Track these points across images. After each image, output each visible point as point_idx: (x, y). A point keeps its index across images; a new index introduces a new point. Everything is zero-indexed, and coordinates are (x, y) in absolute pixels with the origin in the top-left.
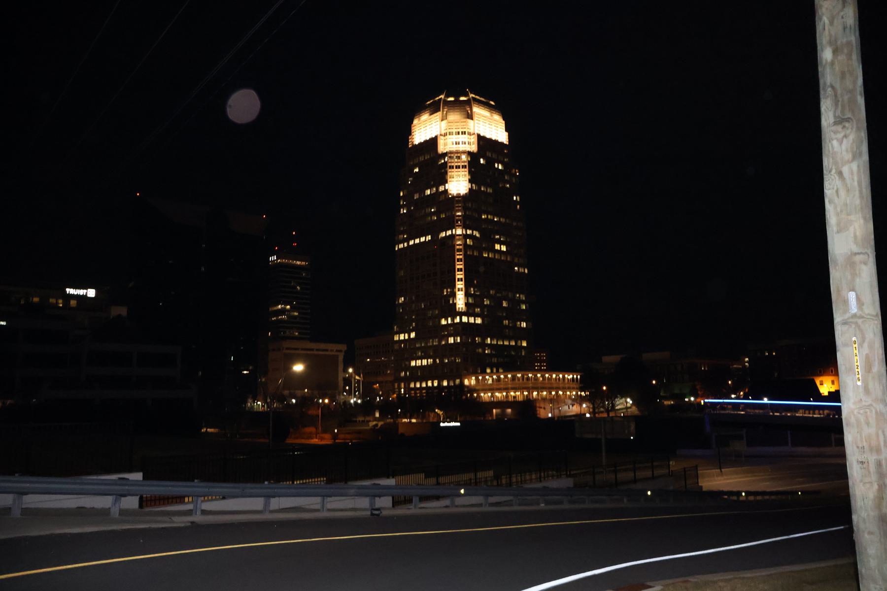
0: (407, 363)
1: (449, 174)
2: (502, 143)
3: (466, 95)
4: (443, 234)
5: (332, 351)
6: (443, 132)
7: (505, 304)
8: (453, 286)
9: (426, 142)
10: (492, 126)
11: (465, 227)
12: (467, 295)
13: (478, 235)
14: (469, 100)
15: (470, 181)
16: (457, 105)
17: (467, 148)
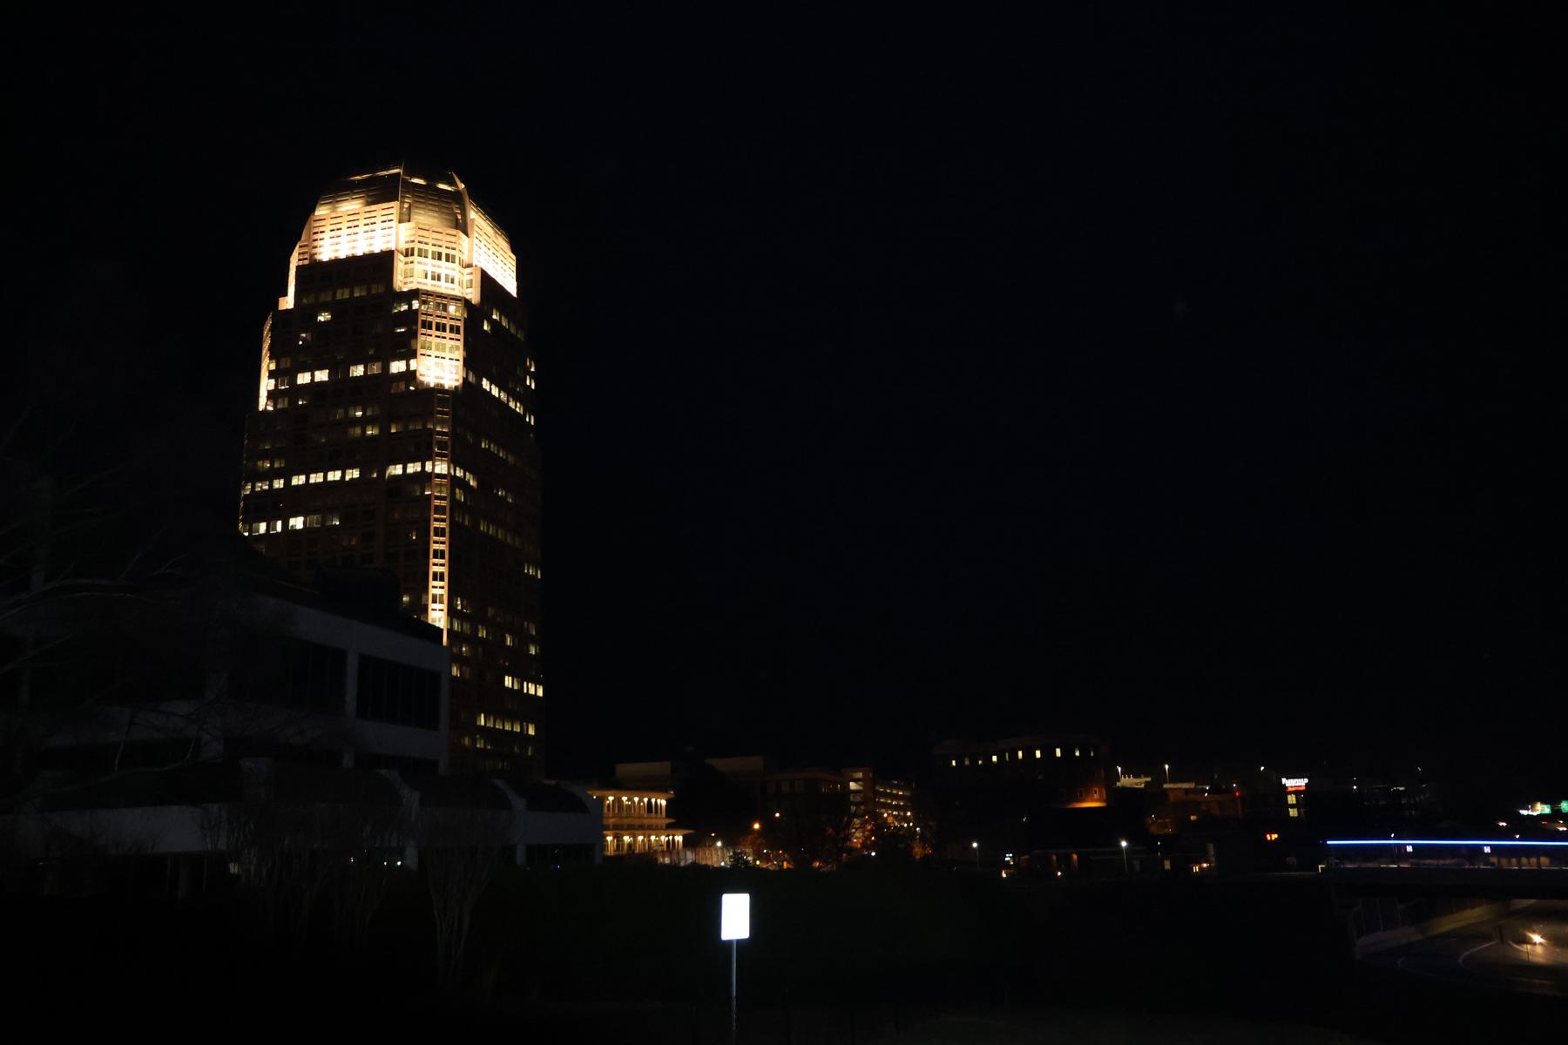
1: (421, 338)
3: (451, 183)
4: (397, 470)
6: (403, 246)
9: (352, 260)
11: (454, 461)
15: (468, 364)
16: (428, 196)
17: (456, 291)
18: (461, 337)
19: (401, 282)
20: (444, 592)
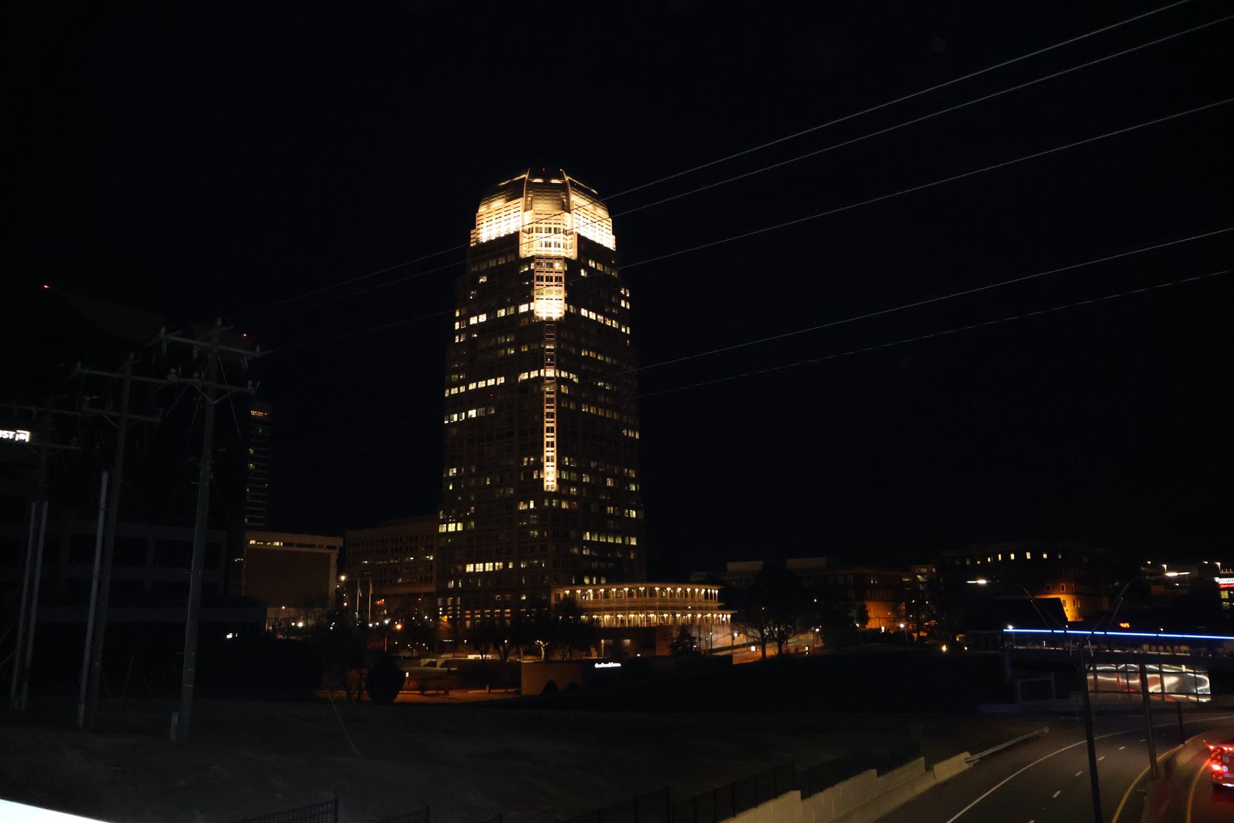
0: (460, 568)
2: (607, 249)
3: (560, 177)
4: (525, 376)
5: (321, 547)
6: (526, 228)
7: (609, 483)
8: (541, 453)
9: (499, 239)
10: (593, 223)
11: (559, 367)
12: (560, 467)
13: (575, 380)
14: (565, 184)
15: (567, 300)
16: (546, 190)
17: (562, 253)
19: (525, 252)
20: (554, 454)
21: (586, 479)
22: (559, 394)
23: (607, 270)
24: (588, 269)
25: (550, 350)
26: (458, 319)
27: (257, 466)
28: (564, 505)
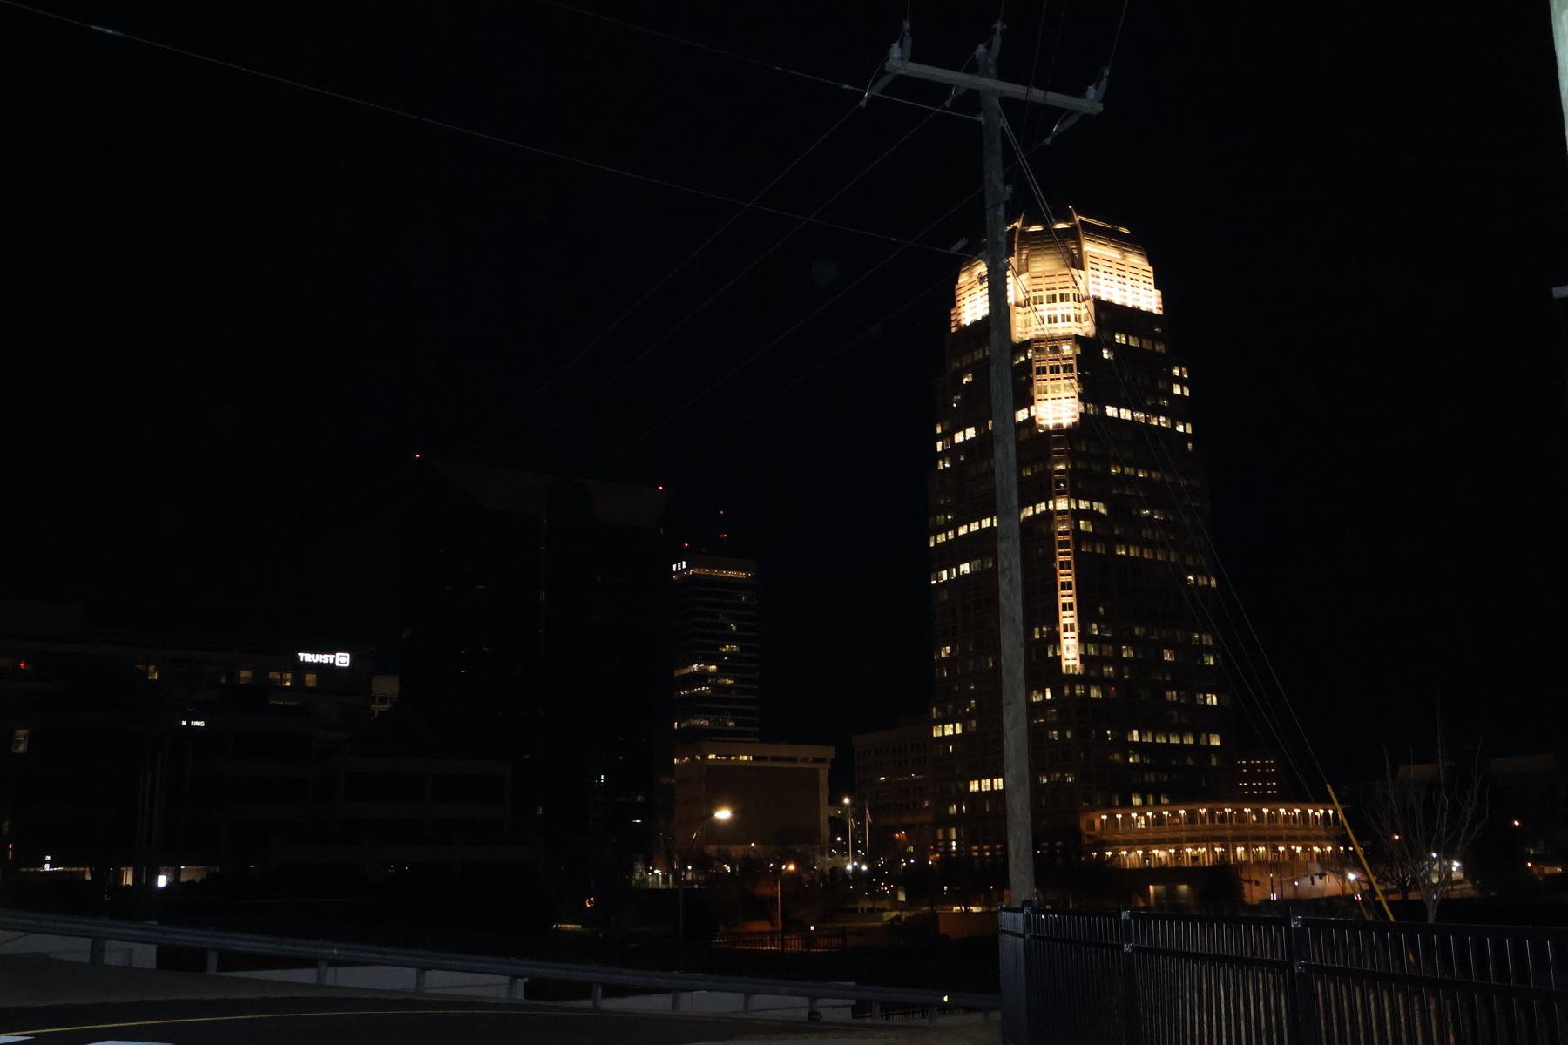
0: (961, 785)
1: (1037, 384)
2: (1149, 314)
3: (1066, 218)
5: (805, 760)
7: (1168, 657)
10: (1126, 280)
11: (1075, 495)
12: (1084, 638)
13: (1103, 511)
15: (1082, 398)
16: (1045, 242)
18: (1075, 373)
21: (1127, 653)
22: (1076, 531)
23: (1147, 345)
24: (1112, 346)
25: (1061, 472)
26: (940, 437)
27: (742, 648)
28: (1094, 693)
